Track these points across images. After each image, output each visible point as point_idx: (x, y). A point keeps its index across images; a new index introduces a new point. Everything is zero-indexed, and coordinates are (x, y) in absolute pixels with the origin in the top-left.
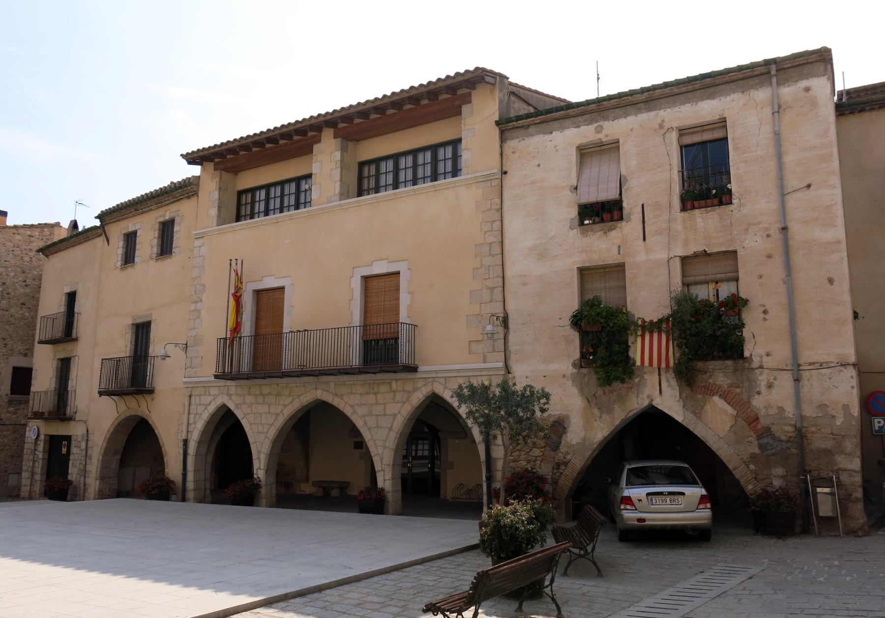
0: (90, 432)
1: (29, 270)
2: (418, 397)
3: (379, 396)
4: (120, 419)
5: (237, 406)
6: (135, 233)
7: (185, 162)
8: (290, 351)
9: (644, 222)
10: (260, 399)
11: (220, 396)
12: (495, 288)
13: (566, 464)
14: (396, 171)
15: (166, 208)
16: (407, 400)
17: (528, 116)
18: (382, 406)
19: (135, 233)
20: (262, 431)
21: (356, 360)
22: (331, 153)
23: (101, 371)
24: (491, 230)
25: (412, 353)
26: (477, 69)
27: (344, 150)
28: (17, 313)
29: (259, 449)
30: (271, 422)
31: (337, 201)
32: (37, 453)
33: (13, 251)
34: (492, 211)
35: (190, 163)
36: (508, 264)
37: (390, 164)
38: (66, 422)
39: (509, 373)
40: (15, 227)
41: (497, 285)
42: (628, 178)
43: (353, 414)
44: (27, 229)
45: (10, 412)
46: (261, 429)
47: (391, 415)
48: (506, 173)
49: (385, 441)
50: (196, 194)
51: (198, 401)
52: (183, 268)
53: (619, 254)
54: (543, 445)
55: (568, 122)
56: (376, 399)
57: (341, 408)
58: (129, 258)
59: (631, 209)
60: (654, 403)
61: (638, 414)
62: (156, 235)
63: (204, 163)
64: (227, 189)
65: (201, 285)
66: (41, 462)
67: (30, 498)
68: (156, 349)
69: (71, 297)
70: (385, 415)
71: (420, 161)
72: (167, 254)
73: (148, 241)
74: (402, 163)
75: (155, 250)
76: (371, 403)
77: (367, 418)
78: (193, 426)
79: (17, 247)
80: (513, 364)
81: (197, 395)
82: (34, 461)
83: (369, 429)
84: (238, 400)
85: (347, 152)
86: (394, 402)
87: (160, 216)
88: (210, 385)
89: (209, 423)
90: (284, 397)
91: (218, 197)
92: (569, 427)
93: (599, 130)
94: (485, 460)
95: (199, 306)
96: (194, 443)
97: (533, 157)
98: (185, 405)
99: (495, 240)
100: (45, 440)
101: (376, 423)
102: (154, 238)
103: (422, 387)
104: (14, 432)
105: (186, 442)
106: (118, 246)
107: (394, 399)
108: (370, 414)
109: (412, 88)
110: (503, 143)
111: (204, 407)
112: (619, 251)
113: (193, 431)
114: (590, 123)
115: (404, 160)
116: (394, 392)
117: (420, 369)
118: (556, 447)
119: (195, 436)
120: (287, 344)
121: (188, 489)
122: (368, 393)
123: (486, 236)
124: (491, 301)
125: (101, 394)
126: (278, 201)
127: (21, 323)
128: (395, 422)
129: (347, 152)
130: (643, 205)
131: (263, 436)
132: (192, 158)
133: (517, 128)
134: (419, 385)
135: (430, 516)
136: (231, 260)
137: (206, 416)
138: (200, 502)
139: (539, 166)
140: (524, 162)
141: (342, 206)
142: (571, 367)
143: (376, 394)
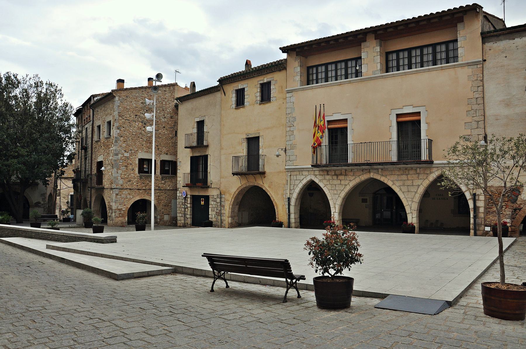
0: (222, 193)
1: (165, 109)
3: (409, 176)
4: (242, 187)
6: (243, 90)
8: (352, 153)
10: (335, 177)
11: (310, 176)
12: (479, 121)
15: (264, 76)
16: (427, 178)
18: (411, 181)
19: (243, 90)
20: (336, 193)
22: (374, 47)
23: (232, 162)
24: (477, 91)
27: (381, 46)
28: (162, 132)
31: (378, 74)
33: (158, 99)
34: (478, 81)
35: (283, 52)
36: (487, 109)
41: (481, 120)
44: (163, 87)
45: (162, 183)
46: (335, 192)
47: (416, 185)
48: (485, 60)
50: (285, 68)
51: (295, 178)
52: (279, 108)
54: (507, 200)
56: (407, 177)
57: (385, 182)
58: (240, 101)
61: (302, 192)
62: (259, 90)
63: (289, 51)
64: (303, 66)
65: (293, 117)
67: (184, 226)
69: (201, 124)
71: (320, 70)
72: (240, 105)
76: (404, 179)
77: (401, 187)
78: (293, 191)
79: (160, 97)
81: (295, 175)
83: (403, 192)
84: (320, 177)
85: (382, 47)
86: (418, 179)
87: (260, 80)
88: (303, 170)
90: (350, 176)
91: (300, 70)
95: (292, 129)
96: (294, 199)
97: (502, 52)
98: (287, 181)
99: (480, 96)
100: (190, 198)
101: (407, 189)
105: (289, 199)
107: (418, 177)
108: (404, 185)
110: (483, 44)
111: (299, 181)
113: (293, 193)
115: (340, 65)
116: (419, 174)
117: (435, 162)
118: (515, 201)
119: (295, 196)
120: (357, 149)
122: (402, 175)
123: (474, 94)
124: (477, 128)
125: (234, 174)
127: (164, 137)
128: (419, 189)
129: (382, 47)
132: (284, 50)
133: (492, 36)
134: (434, 171)
136: (320, 105)
137: (301, 186)
140: (497, 55)
141: (341, 83)
143: (407, 175)
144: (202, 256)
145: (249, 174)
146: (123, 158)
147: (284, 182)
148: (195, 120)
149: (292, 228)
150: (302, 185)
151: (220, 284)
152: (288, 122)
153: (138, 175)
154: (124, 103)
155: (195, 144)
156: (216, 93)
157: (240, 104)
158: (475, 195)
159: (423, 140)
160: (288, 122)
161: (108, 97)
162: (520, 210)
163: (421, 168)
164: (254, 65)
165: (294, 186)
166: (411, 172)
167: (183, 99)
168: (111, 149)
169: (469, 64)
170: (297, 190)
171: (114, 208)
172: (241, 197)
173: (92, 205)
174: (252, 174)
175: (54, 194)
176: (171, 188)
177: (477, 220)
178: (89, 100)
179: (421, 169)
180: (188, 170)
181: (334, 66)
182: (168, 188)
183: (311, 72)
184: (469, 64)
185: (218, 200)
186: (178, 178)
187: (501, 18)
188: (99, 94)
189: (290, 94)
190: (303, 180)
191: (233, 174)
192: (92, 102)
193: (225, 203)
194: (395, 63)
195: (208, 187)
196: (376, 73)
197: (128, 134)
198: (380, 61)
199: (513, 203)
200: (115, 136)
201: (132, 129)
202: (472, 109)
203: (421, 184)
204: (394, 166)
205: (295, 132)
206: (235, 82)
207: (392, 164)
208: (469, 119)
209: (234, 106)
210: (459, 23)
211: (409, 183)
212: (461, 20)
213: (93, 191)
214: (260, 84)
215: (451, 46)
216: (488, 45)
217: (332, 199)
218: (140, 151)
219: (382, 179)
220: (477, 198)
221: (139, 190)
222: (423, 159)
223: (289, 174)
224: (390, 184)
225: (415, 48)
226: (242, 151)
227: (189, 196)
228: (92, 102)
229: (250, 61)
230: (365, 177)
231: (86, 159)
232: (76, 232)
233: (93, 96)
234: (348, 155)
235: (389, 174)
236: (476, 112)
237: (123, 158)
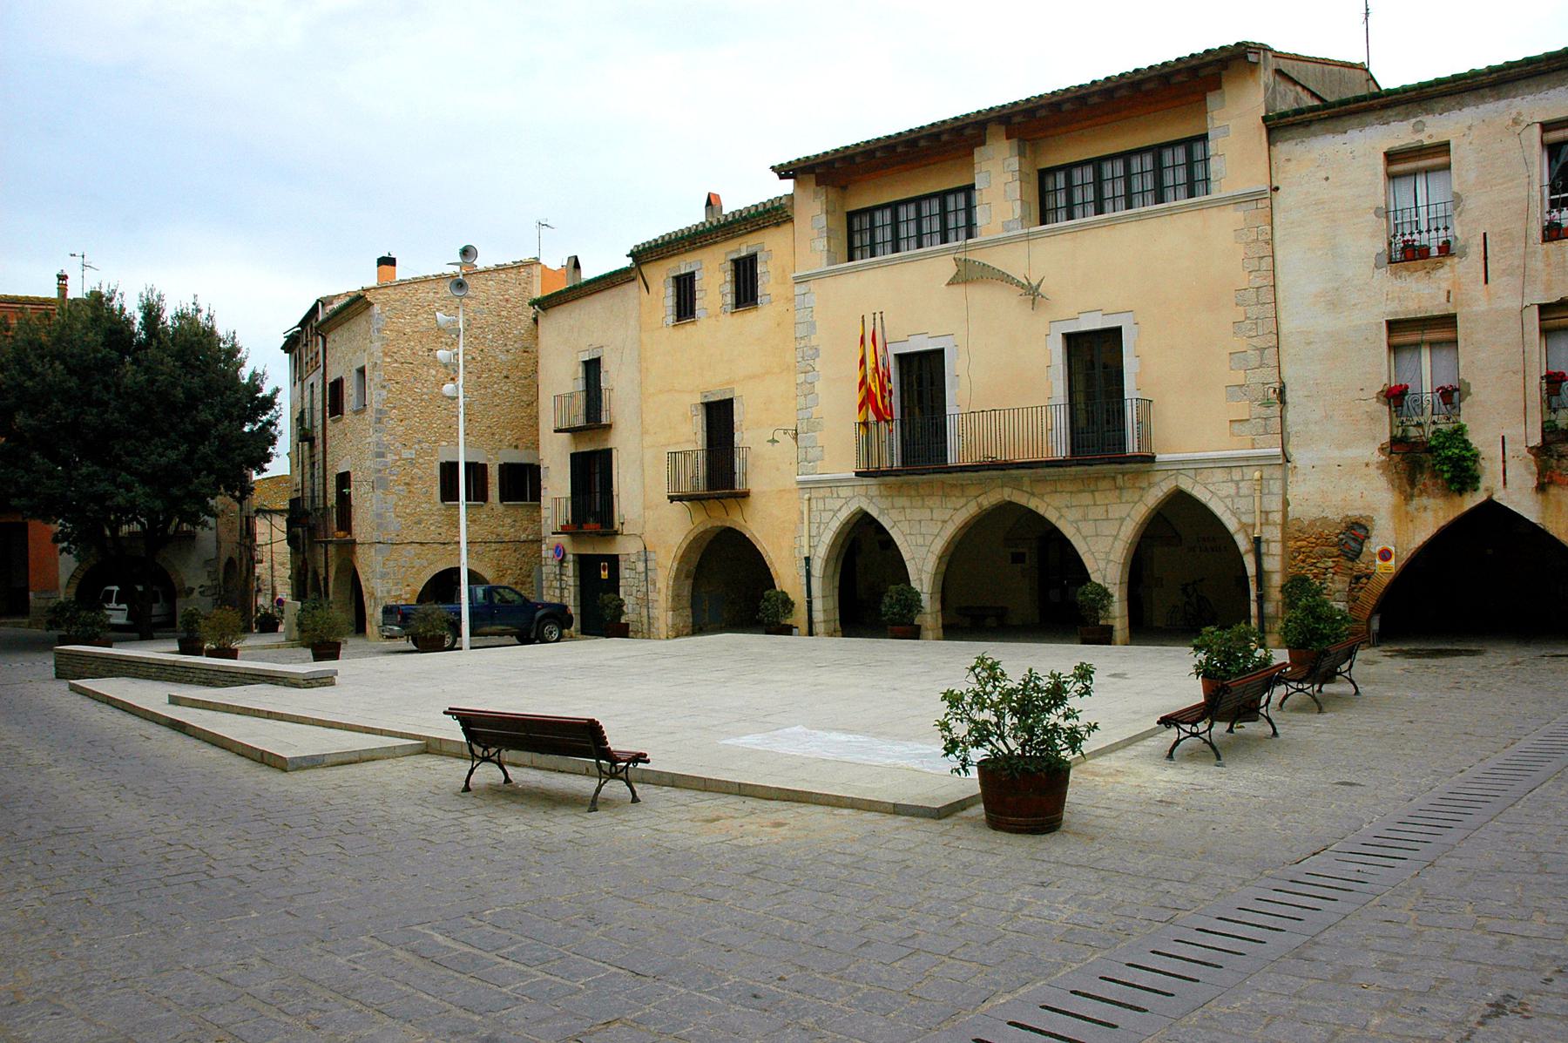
2: (1155, 495)
4: (697, 531)
5: (881, 511)
6: (691, 276)
7: (775, 176)
9: (1486, 258)
11: (856, 499)
13: (1368, 576)
14: (1158, 170)
15: (740, 240)
17: (1312, 109)
19: (691, 276)
21: (1061, 451)
22: (1004, 159)
25: (1144, 435)
26: (1238, 44)
27: (1021, 154)
28: (501, 389)
29: (920, 567)
30: (936, 531)
32: (565, 578)
34: (1259, 244)
35: (781, 177)
36: (1282, 315)
37: (1089, 173)
38: (609, 537)
39: (1288, 461)
40: (499, 269)
42: (1463, 197)
43: (1059, 518)
46: (920, 540)
48: (1277, 189)
49: (1108, 553)
50: (790, 220)
51: (821, 506)
53: (1448, 301)
55: (1371, 118)
57: (1041, 511)
58: (685, 307)
59: (1467, 240)
60: (1495, 498)
66: (572, 589)
68: (744, 436)
69: (592, 368)
70: (1107, 519)
71: (1077, 180)
73: (714, 282)
74: (1107, 170)
75: (730, 299)
77: (1079, 523)
78: (816, 539)
80: (1291, 449)
82: (562, 589)
83: (1085, 538)
84: (884, 503)
87: (732, 252)
89: (838, 535)
92: (1373, 529)
93: (1418, 129)
94: (1254, 574)
95: (810, 377)
98: (802, 513)
99: (1265, 283)
100: (574, 561)
102: (726, 282)
103: (1162, 481)
104: (515, 551)
106: (665, 297)
109: (1137, 71)
110: (1272, 147)
111: (832, 513)
112: (1448, 297)
114: (1407, 117)
117: (1159, 457)
121: (815, 620)
125: (672, 499)
126: (912, 226)
128: (1123, 528)
130: (1485, 234)
131: (925, 550)
132: (784, 171)
135: (961, 639)
137: (835, 525)
138: (831, 636)
139: (1327, 179)
142: (1377, 453)
143: (1093, 492)
144: (445, 713)
145: (709, 498)
146: (398, 463)
147: (796, 517)
148: (577, 358)
149: (817, 634)
150: (838, 524)
151: (488, 774)
152: (800, 359)
153: (440, 505)
154: (396, 320)
155: (580, 421)
156: (626, 286)
157: (685, 315)
158: (1258, 541)
159: (1129, 402)
160: (800, 359)
161: (357, 304)
162: (1368, 579)
163: (1127, 473)
164: (730, 206)
165: (818, 527)
166: (1103, 484)
167: (547, 304)
168: (369, 440)
169: (1236, 200)
170: (827, 537)
171: (379, 595)
172: (695, 558)
173: (331, 585)
174: (717, 498)
175: (241, 559)
176: (530, 537)
177: (1265, 606)
178: (314, 311)
179: (1126, 478)
180: (566, 491)
181: (1119, 167)
182: (523, 537)
183: (1050, 187)
184: (1236, 200)
185: (641, 567)
186: (543, 511)
187: (1358, 61)
188: (339, 295)
189: (803, 285)
190: (840, 510)
191: (669, 497)
192: (321, 317)
193: (656, 575)
194: (1061, 200)
195: (616, 533)
196: (1011, 226)
197: (410, 400)
198: (1021, 196)
199: (1352, 560)
200: (375, 406)
201: (420, 385)
202: (1247, 318)
203: (1128, 515)
204: (1061, 469)
205: (818, 386)
206: (671, 256)
207: (1048, 466)
208: (1239, 344)
209: (671, 319)
210: (1211, 91)
211: (1098, 512)
212: (1215, 84)
213: (332, 549)
214: (732, 260)
215: (1198, 149)
216: (1282, 149)
217: (913, 558)
218: (444, 443)
219: (1033, 504)
220: (1264, 548)
221: (444, 544)
222: (1131, 451)
223: (807, 496)
224: (1052, 516)
225: (1112, 157)
226: (693, 438)
227: (570, 557)
228: (321, 317)
229: (717, 197)
230: (990, 499)
231: (313, 464)
232: (262, 660)
233: (323, 302)
234: (946, 442)
235: (1048, 490)
236: (1256, 324)
237: (398, 463)
